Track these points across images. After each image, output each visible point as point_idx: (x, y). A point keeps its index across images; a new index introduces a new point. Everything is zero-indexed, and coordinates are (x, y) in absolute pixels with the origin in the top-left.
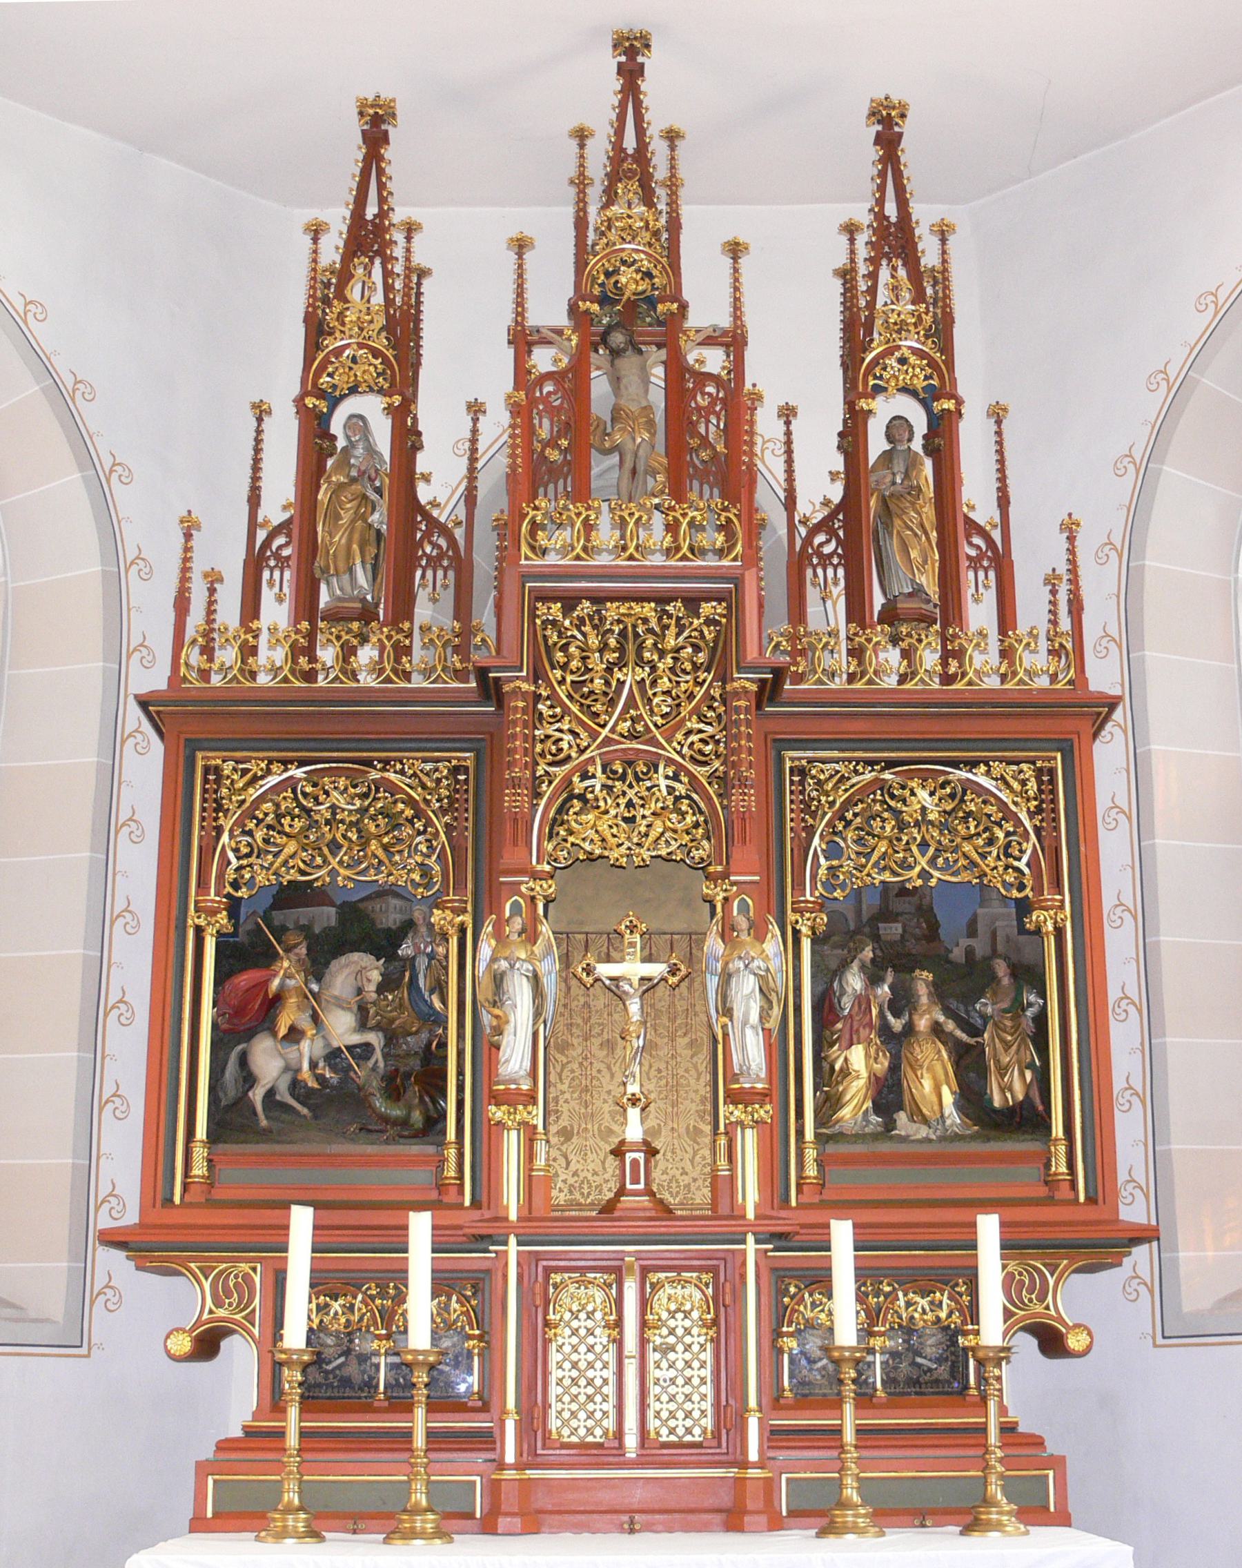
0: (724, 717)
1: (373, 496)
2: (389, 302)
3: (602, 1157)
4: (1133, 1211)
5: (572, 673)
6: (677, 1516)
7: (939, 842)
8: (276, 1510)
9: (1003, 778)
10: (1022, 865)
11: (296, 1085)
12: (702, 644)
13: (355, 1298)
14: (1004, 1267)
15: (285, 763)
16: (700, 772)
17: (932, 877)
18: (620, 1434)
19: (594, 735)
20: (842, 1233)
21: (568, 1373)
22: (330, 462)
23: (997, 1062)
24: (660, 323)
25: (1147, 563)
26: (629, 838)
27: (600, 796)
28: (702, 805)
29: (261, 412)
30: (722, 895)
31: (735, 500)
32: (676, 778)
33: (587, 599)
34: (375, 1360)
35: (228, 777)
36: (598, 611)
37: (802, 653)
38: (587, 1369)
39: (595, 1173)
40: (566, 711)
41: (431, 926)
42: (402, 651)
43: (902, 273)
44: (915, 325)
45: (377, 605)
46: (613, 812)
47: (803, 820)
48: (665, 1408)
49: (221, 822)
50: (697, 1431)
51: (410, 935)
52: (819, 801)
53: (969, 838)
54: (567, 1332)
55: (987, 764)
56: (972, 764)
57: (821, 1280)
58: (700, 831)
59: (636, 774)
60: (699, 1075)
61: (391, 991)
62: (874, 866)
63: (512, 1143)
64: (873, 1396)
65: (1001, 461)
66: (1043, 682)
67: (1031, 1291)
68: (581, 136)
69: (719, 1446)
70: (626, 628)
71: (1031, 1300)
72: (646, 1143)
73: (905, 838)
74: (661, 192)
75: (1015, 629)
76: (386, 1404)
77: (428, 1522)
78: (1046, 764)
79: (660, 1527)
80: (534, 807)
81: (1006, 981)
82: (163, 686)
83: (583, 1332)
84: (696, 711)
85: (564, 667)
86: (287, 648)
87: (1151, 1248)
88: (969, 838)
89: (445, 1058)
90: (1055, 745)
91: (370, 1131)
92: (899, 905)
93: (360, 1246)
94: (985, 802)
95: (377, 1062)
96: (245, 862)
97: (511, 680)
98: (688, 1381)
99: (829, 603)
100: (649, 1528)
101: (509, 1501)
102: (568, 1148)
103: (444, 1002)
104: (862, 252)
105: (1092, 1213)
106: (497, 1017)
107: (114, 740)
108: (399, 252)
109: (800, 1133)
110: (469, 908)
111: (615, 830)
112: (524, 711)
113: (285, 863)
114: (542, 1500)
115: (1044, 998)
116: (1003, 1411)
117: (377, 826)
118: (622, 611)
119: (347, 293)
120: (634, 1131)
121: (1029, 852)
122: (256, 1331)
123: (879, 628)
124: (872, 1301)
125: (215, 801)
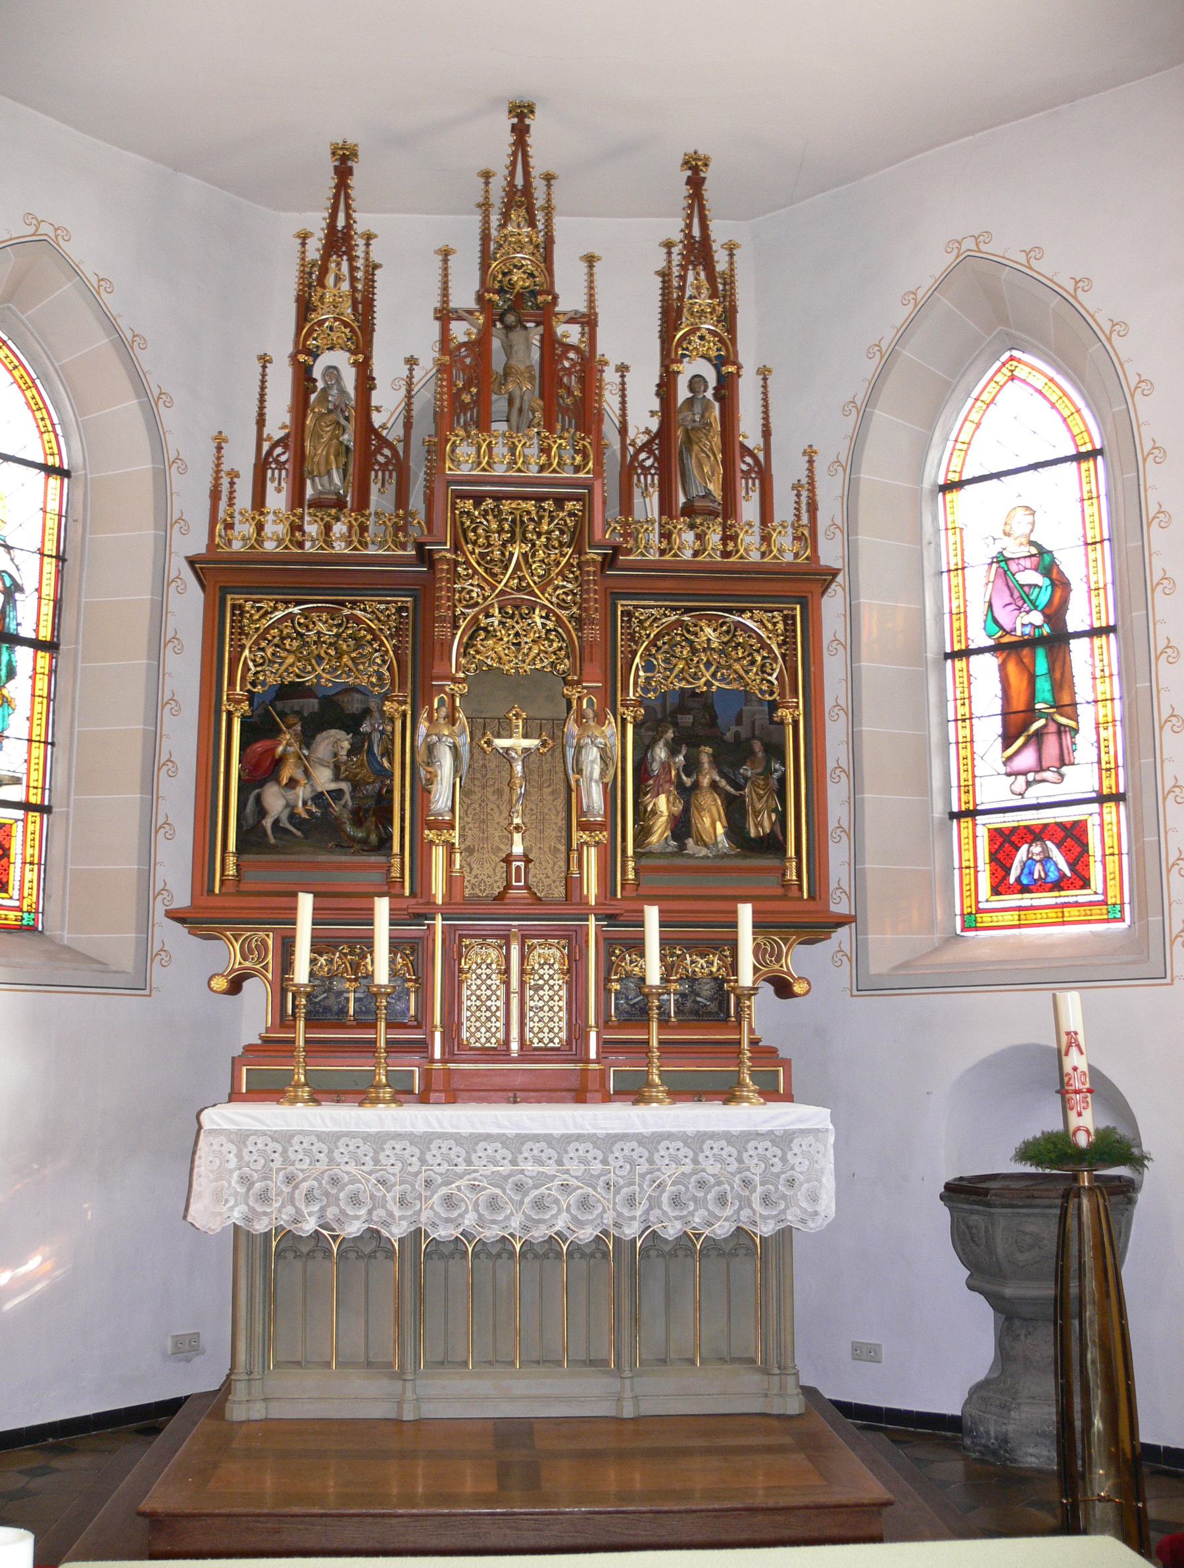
0: (580, 578)
1: (343, 422)
2: (354, 289)
3: (493, 864)
4: (840, 906)
5: (480, 546)
6: (546, 1093)
7: (719, 663)
8: (290, 1085)
9: (761, 622)
10: (773, 679)
11: (293, 816)
12: (565, 529)
13: (334, 955)
14: (754, 939)
15: (287, 603)
16: (563, 614)
17: (713, 685)
18: (507, 1041)
19: (493, 588)
20: (652, 915)
21: (474, 1002)
22: (313, 397)
23: (753, 807)
24: (538, 308)
25: (862, 475)
26: (516, 657)
27: (498, 628)
28: (565, 636)
29: (265, 360)
30: (577, 695)
31: (588, 432)
32: (547, 617)
33: (490, 498)
34: (346, 995)
35: (248, 612)
36: (497, 506)
37: (630, 535)
38: (486, 1001)
39: (489, 876)
40: (475, 572)
41: (382, 713)
42: (363, 529)
43: (702, 275)
44: (711, 313)
45: (346, 496)
46: (506, 639)
47: (630, 646)
48: (536, 1026)
49: (244, 642)
50: (556, 1040)
51: (368, 718)
52: (640, 634)
53: (738, 660)
54: (474, 976)
55: (751, 611)
56: (741, 611)
57: (637, 946)
58: (563, 653)
59: (521, 615)
60: (558, 813)
61: (355, 755)
62: (675, 677)
63: (438, 855)
64: (668, 1021)
65: (766, 406)
66: (788, 557)
67: (771, 956)
68: (487, 176)
69: (571, 1050)
70: (516, 518)
71: (771, 961)
72: (525, 855)
73: (696, 659)
74: (540, 216)
75: (772, 521)
76: (355, 1023)
77: (387, 1093)
78: (790, 612)
79: (533, 1100)
80: (454, 635)
81: (760, 755)
82: (203, 551)
83: (484, 977)
84: (560, 573)
85: (475, 543)
86: (288, 526)
87: (850, 928)
88: (738, 660)
89: (392, 799)
90: (796, 600)
91: (342, 847)
92: (691, 703)
93: (332, 921)
94: (749, 636)
95: (346, 802)
96: (258, 669)
97: (440, 551)
98: (551, 1008)
99: (647, 500)
100: (526, 1100)
101: (437, 1082)
102: (471, 859)
103: (391, 762)
104: (676, 259)
105: (811, 906)
106: (430, 772)
107: (162, 582)
108: (360, 252)
109: (624, 850)
110: (409, 700)
111: (506, 652)
112: (448, 571)
113: (286, 670)
114: (457, 1083)
115: (784, 766)
116: (751, 1031)
117: (348, 646)
118: (514, 506)
119: (326, 282)
120: (518, 849)
121: (778, 670)
122: (270, 976)
123: (682, 519)
124: (670, 960)
125: (240, 628)
